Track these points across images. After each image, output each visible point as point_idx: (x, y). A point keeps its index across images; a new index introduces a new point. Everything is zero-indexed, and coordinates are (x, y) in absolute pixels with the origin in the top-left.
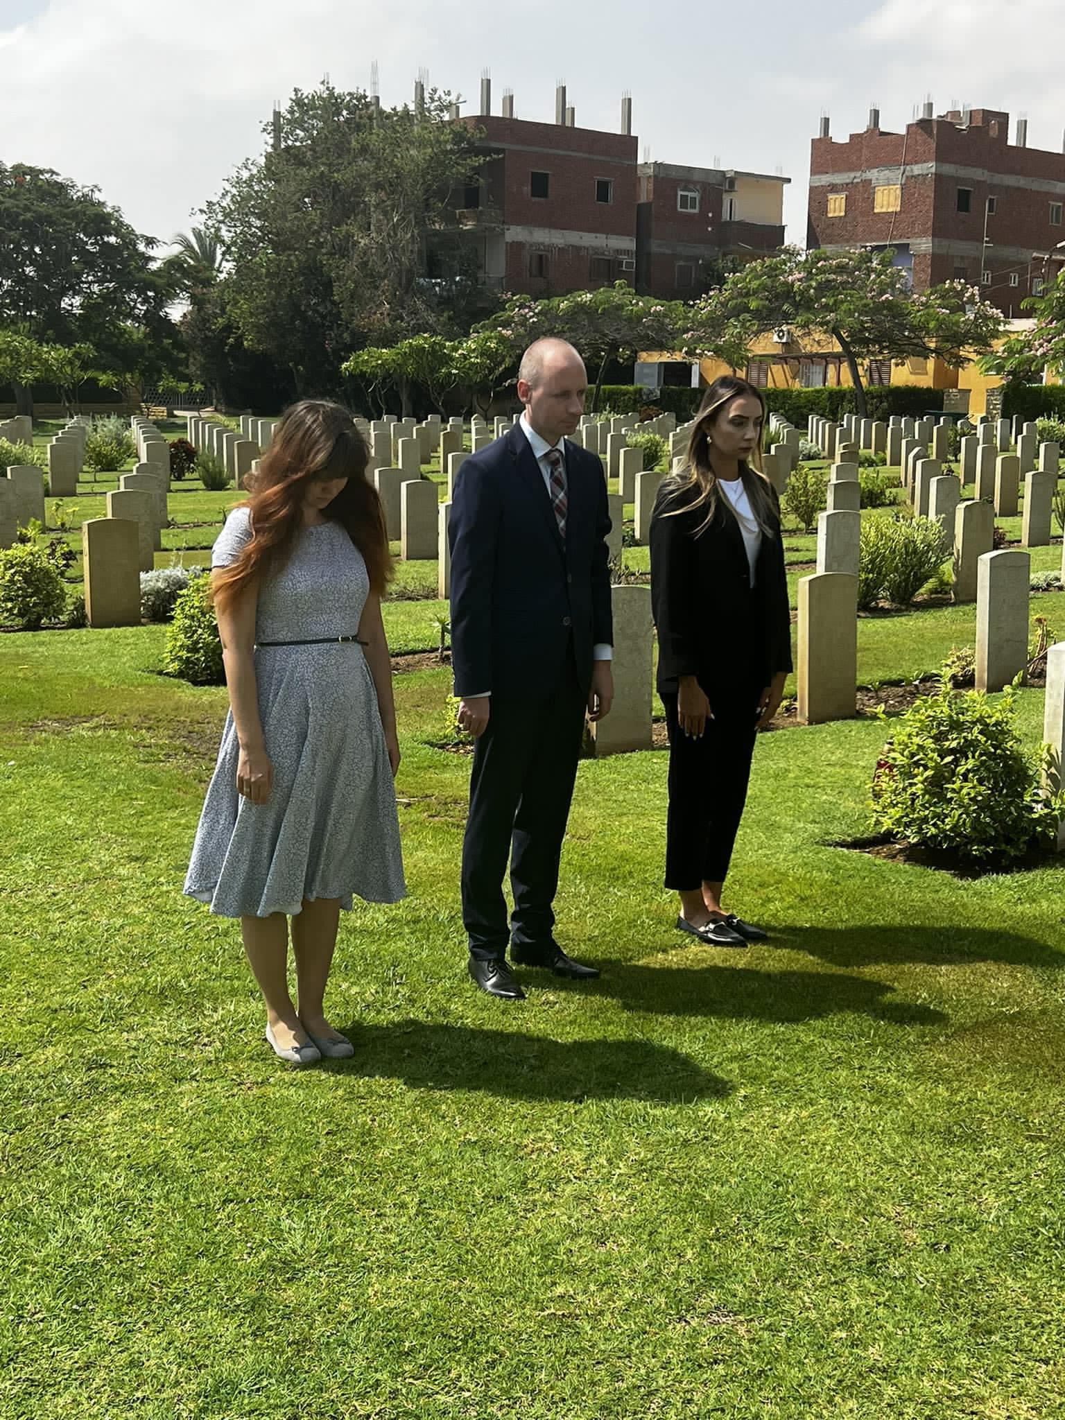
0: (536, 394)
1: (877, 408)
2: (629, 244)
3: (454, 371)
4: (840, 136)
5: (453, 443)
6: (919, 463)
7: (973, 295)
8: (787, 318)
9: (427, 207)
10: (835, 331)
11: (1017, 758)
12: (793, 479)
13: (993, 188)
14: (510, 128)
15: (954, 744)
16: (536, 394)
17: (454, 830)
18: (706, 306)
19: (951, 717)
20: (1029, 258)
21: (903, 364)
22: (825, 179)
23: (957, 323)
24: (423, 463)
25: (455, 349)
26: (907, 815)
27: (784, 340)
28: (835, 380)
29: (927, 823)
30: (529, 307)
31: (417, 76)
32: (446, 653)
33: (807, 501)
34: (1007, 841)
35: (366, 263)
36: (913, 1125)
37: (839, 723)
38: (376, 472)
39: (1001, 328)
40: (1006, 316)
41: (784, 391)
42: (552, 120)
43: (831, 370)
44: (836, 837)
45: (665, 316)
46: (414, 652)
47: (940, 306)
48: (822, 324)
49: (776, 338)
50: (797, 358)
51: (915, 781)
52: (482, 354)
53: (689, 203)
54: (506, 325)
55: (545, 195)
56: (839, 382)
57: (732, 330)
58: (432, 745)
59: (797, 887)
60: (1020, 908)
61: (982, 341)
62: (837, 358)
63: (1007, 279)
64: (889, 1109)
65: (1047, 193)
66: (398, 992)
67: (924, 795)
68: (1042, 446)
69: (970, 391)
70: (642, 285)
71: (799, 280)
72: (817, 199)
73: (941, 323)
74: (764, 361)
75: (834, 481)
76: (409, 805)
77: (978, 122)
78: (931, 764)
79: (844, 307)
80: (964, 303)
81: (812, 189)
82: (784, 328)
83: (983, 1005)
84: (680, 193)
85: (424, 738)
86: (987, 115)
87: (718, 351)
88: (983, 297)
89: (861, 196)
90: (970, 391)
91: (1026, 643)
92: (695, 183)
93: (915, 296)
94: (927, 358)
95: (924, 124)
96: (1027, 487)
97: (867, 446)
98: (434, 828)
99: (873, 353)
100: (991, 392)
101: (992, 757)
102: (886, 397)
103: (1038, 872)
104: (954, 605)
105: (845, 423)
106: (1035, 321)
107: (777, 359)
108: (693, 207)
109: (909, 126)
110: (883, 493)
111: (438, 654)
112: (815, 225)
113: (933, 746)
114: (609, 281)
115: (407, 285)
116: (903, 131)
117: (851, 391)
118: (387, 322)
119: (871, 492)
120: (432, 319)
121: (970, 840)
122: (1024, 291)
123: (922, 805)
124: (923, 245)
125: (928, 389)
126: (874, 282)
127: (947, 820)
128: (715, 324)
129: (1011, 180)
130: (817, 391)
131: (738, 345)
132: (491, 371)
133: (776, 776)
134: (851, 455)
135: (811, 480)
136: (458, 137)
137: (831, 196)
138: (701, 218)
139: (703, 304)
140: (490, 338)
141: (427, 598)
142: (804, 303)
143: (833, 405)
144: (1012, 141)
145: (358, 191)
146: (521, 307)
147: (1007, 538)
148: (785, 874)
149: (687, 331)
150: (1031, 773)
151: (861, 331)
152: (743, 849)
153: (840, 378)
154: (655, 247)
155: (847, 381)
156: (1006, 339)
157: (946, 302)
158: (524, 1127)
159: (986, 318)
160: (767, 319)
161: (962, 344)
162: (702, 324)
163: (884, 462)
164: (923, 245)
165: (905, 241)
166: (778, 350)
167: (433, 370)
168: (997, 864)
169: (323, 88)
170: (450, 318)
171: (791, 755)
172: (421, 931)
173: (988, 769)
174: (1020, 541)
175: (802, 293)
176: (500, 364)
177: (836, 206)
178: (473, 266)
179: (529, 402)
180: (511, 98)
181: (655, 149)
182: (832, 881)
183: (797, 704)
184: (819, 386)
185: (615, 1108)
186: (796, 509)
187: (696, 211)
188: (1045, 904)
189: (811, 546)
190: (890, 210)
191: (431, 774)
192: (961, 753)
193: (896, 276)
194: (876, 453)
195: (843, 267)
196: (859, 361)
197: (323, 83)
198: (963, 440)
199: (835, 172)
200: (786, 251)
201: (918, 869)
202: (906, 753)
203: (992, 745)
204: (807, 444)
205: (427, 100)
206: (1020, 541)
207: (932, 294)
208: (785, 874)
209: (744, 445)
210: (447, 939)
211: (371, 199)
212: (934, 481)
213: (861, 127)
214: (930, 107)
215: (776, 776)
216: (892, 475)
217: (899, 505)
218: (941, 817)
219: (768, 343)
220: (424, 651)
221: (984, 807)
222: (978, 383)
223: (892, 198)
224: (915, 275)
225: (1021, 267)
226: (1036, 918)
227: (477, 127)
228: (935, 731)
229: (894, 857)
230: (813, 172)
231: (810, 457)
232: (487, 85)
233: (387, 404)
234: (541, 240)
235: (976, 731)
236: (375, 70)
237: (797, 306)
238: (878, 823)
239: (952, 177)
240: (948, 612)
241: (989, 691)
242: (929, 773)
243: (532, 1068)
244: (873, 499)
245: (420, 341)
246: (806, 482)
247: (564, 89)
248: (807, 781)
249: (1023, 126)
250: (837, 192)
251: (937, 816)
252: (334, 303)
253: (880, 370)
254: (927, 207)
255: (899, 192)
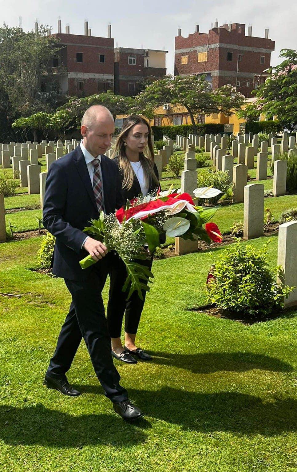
0: (91, 133)
1: (201, 132)
2: (112, 77)
3: (51, 125)
4: (185, 35)
5: (50, 150)
6: (218, 151)
7: (234, 90)
8: (168, 101)
9: (40, 67)
10: (186, 105)
11: (267, 272)
12: (172, 158)
13: (240, 51)
14: (68, 37)
15: (241, 268)
16: (91, 133)
17: (37, 308)
18: (139, 98)
19: (239, 256)
20: (254, 76)
21: (209, 116)
22: (180, 51)
23: (229, 100)
24: (39, 157)
25: (51, 117)
26: (222, 298)
27: (167, 109)
28: (186, 122)
29: (230, 301)
30: (77, 101)
31: (35, 20)
32: (41, 230)
33: (177, 166)
34: (264, 308)
35: (20, 88)
36: (234, 459)
37: (192, 254)
38: (20, 162)
39: (244, 101)
40: (246, 97)
41: (168, 127)
42: (83, 34)
43: (184, 118)
44: (192, 306)
45: (125, 102)
46: (29, 231)
47: (223, 94)
48: (180, 102)
49: (164, 108)
50: (172, 115)
51: (225, 283)
52: (61, 118)
53: (132, 61)
54: (69, 107)
55: (82, 61)
56: (187, 123)
57: (148, 107)
58: (32, 270)
59: (177, 331)
60: (271, 339)
61: (238, 106)
62: (186, 114)
63: (246, 84)
64: (222, 449)
65: (259, 53)
66: (6, 389)
67: (229, 290)
68: (262, 143)
69: (234, 124)
70: (117, 91)
71: (172, 87)
72: (178, 59)
73: (224, 100)
74: (160, 116)
75: (186, 159)
76: (20, 297)
77: (234, 28)
78: (232, 277)
79: (188, 96)
80: (231, 93)
81: (176, 55)
82: (167, 104)
83: (260, 389)
84: (129, 58)
85: (30, 267)
86: (238, 25)
87: (282, 294)
88: (238, 91)
89: (193, 56)
90: (234, 124)
91: (263, 219)
92: (134, 54)
93: (213, 91)
94: (218, 113)
95: (215, 30)
96: (258, 158)
97: (198, 145)
98: (29, 308)
99: (199, 112)
100: (241, 124)
101: (257, 273)
102: (204, 127)
103: (277, 320)
104: (233, 204)
105: (189, 137)
106: (257, 98)
107: (166, 116)
108: (134, 63)
109: (210, 31)
110: (204, 162)
111: (38, 231)
112: (177, 67)
113: (232, 269)
114: (105, 90)
115: (34, 95)
116: (208, 33)
117: (191, 126)
118: (28, 108)
119: (200, 162)
120: (43, 107)
121: (248, 308)
122: (252, 88)
123: (228, 294)
124: (216, 73)
125: (219, 124)
126: (199, 87)
127: (239, 300)
128: (142, 104)
129: (246, 49)
130: (179, 127)
131: (151, 111)
132: (64, 124)
133: (167, 279)
134: (192, 149)
135: (178, 158)
136: (51, 42)
137: (183, 57)
138: (137, 67)
139: (138, 97)
140: (64, 112)
141: (36, 208)
142: (175, 95)
143: (185, 131)
144: (247, 34)
145: (16, 63)
146: (74, 101)
147: (251, 178)
148: (172, 325)
149: (132, 107)
150: (273, 278)
151: (194, 104)
152: (154, 313)
153: (187, 121)
154: (121, 78)
155: (189, 122)
156: (246, 106)
157: (224, 93)
158: (55, 464)
159: (239, 98)
160: (161, 101)
161: (230, 108)
162: (138, 104)
163: (204, 151)
164: (216, 73)
165: (209, 72)
166: (165, 113)
167: (44, 125)
168: (261, 318)
169: (4, 26)
170: (49, 106)
171: (173, 269)
172: (19, 357)
173: (255, 278)
174: (256, 178)
175: (173, 92)
176: (67, 121)
177: (185, 60)
178: (57, 87)
179: (86, 136)
180: (69, 27)
181: (121, 42)
182: (192, 328)
183: (175, 247)
184: (180, 125)
185: (97, 452)
186: (173, 170)
187: (135, 64)
188: (282, 336)
189: (179, 183)
190: (204, 61)
191: (31, 283)
192: (245, 271)
193: (206, 84)
194: (201, 148)
195: (188, 82)
196: (194, 115)
197: (4, 24)
198: (233, 142)
199: (183, 48)
200: (167, 77)
201: (227, 320)
202: (221, 272)
203: (257, 268)
204: (176, 145)
205: (39, 28)
206: (256, 178)
207: (219, 90)
208: (172, 325)
209: (140, 146)
210: (29, 361)
211: (21, 65)
212: (224, 157)
213: (193, 31)
214: (217, 23)
215: (167, 279)
216: (207, 155)
217: (210, 166)
218: (237, 299)
219: (162, 110)
220: (33, 230)
221: (254, 294)
222: (237, 121)
223: (204, 57)
224: (213, 84)
225: (251, 80)
226: (279, 343)
227: (57, 38)
228: (233, 263)
229: (217, 314)
230: (176, 49)
231: (177, 150)
232: (60, 22)
233: (28, 137)
234: (81, 77)
235: (250, 262)
236: (20, 19)
237: (171, 96)
238: (210, 300)
239: (226, 48)
240: (231, 207)
241: (249, 239)
242: (231, 280)
243: (61, 430)
244: (201, 165)
245: (39, 114)
246: (176, 159)
247: (87, 22)
248: (180, 281)
249: (250, 28)
250: (185, 55)
251: (234, 298)
252: (9, 102)
253: (201, 117)
254: (217, 59)
255: (207, 54)
